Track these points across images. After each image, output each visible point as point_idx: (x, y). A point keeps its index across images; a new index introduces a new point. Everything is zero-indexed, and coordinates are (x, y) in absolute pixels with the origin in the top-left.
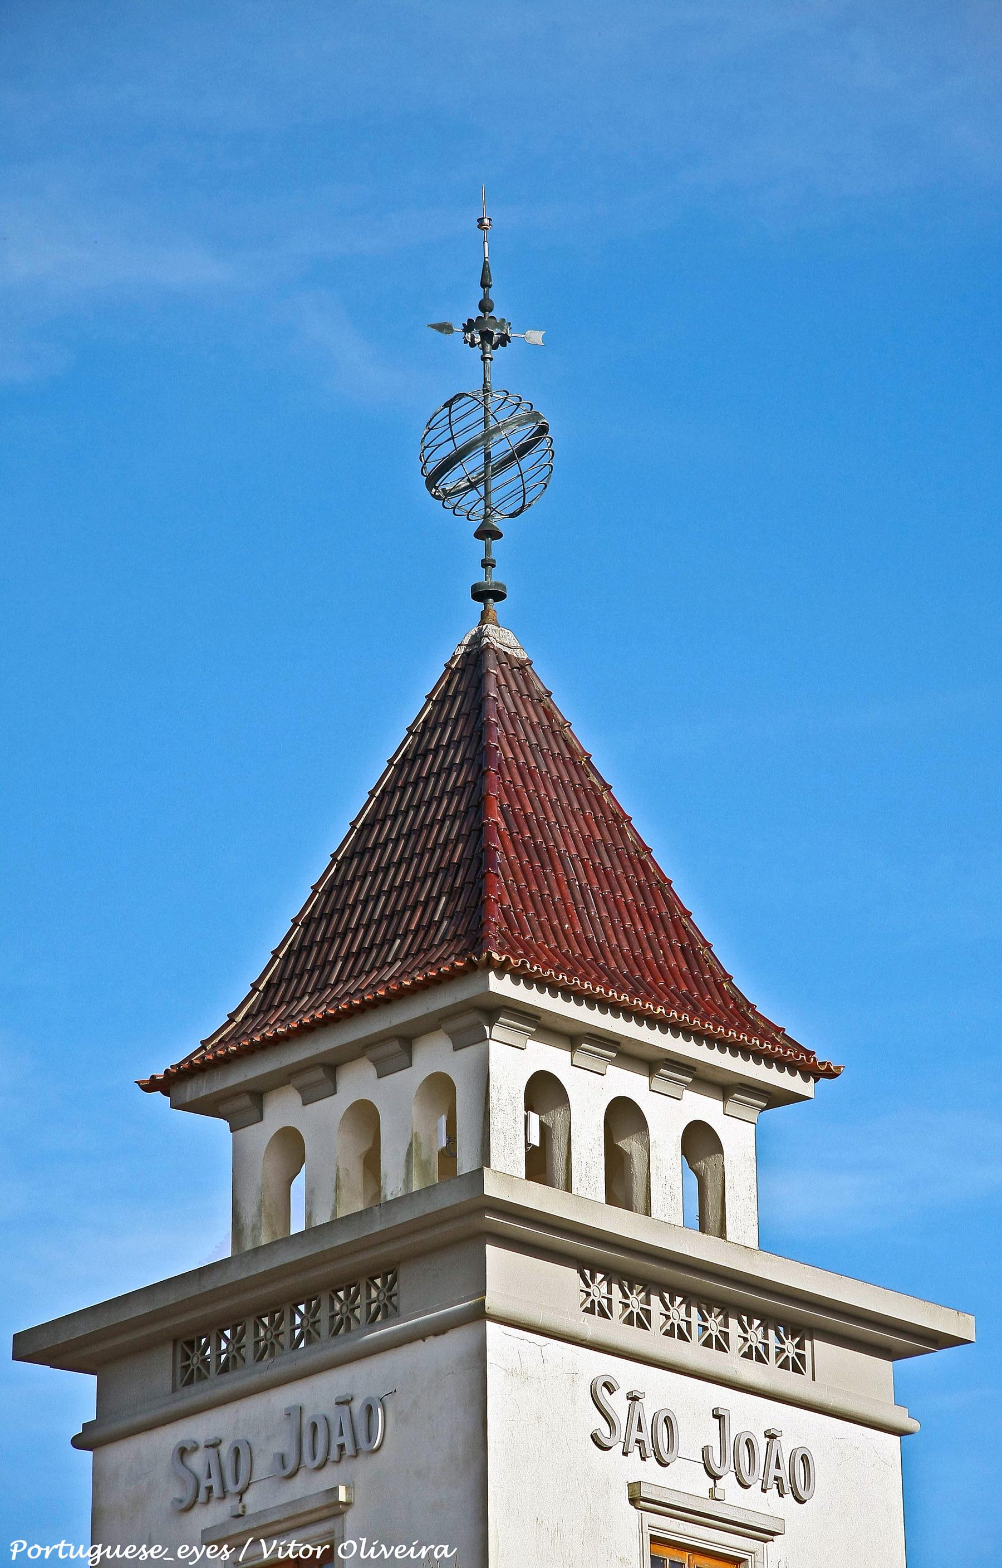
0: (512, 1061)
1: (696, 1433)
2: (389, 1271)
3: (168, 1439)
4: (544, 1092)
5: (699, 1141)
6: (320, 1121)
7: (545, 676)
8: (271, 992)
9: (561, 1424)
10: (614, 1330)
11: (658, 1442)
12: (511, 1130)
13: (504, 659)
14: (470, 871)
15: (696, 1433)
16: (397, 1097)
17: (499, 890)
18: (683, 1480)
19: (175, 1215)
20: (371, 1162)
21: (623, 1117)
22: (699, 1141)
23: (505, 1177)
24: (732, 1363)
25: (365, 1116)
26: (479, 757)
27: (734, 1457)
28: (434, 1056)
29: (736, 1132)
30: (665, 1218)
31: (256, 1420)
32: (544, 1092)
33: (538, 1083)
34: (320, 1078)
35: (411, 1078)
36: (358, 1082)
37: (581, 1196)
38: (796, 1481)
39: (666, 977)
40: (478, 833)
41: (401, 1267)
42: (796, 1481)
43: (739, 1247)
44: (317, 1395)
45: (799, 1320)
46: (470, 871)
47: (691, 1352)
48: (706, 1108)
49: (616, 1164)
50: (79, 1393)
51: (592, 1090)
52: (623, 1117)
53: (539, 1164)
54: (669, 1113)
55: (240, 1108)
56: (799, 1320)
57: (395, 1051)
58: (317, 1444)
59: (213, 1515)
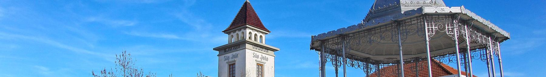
0: (248, 31)
1: (260, 56)
2: (239, 45)
3: (223, 56)
4: (250, 33)
5: (261, 37)
6: (235, 35)
7: (251, 4)
8: (231, 25)
9: (251, 57)
10: (255, 49)
11: (258, 57)
12: (248, 36)
13: (374, 23)
14: (245, 18)
15: (260, 56)
16: (240, 33)
17: (248, 19)
18: (259, 59)
19: (224, 40)
20: (238, 37)
21: (256, 35)
22: (261, 37)
23: (247, 39)
24: (263, 52)
25: (238, 34)
26: (246, 9)
27: (263, 58)
28: (243, 30)
29: (264, 36)
30: (258, 42)
31: (230, 55)
32: (250, 33)
33: (250, 33)
34: (235, 31)
35: (236, 33)
36: (237, 32)
37: (253, 40)
38: (267, 59)
39: (259, 25)
40: (246, 15)
41: (241, 44)
42: (267, 59)
43: (264, 44)
44: (234, 53)
45: (268, 49)
46: (245, 18)
47: (260, 51)
48: (262, 34)
49: (255, 38)
50: (218, 52)
51: (254, 33)
52: (256, 35)
53: (250, 38)
54: (259, 35)
55: (229, 33)
56: (268, 49)
57: (240, 30)
58: (236, 56)
59: (227, 61)
